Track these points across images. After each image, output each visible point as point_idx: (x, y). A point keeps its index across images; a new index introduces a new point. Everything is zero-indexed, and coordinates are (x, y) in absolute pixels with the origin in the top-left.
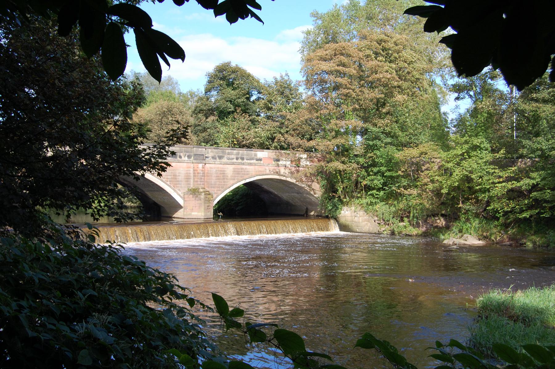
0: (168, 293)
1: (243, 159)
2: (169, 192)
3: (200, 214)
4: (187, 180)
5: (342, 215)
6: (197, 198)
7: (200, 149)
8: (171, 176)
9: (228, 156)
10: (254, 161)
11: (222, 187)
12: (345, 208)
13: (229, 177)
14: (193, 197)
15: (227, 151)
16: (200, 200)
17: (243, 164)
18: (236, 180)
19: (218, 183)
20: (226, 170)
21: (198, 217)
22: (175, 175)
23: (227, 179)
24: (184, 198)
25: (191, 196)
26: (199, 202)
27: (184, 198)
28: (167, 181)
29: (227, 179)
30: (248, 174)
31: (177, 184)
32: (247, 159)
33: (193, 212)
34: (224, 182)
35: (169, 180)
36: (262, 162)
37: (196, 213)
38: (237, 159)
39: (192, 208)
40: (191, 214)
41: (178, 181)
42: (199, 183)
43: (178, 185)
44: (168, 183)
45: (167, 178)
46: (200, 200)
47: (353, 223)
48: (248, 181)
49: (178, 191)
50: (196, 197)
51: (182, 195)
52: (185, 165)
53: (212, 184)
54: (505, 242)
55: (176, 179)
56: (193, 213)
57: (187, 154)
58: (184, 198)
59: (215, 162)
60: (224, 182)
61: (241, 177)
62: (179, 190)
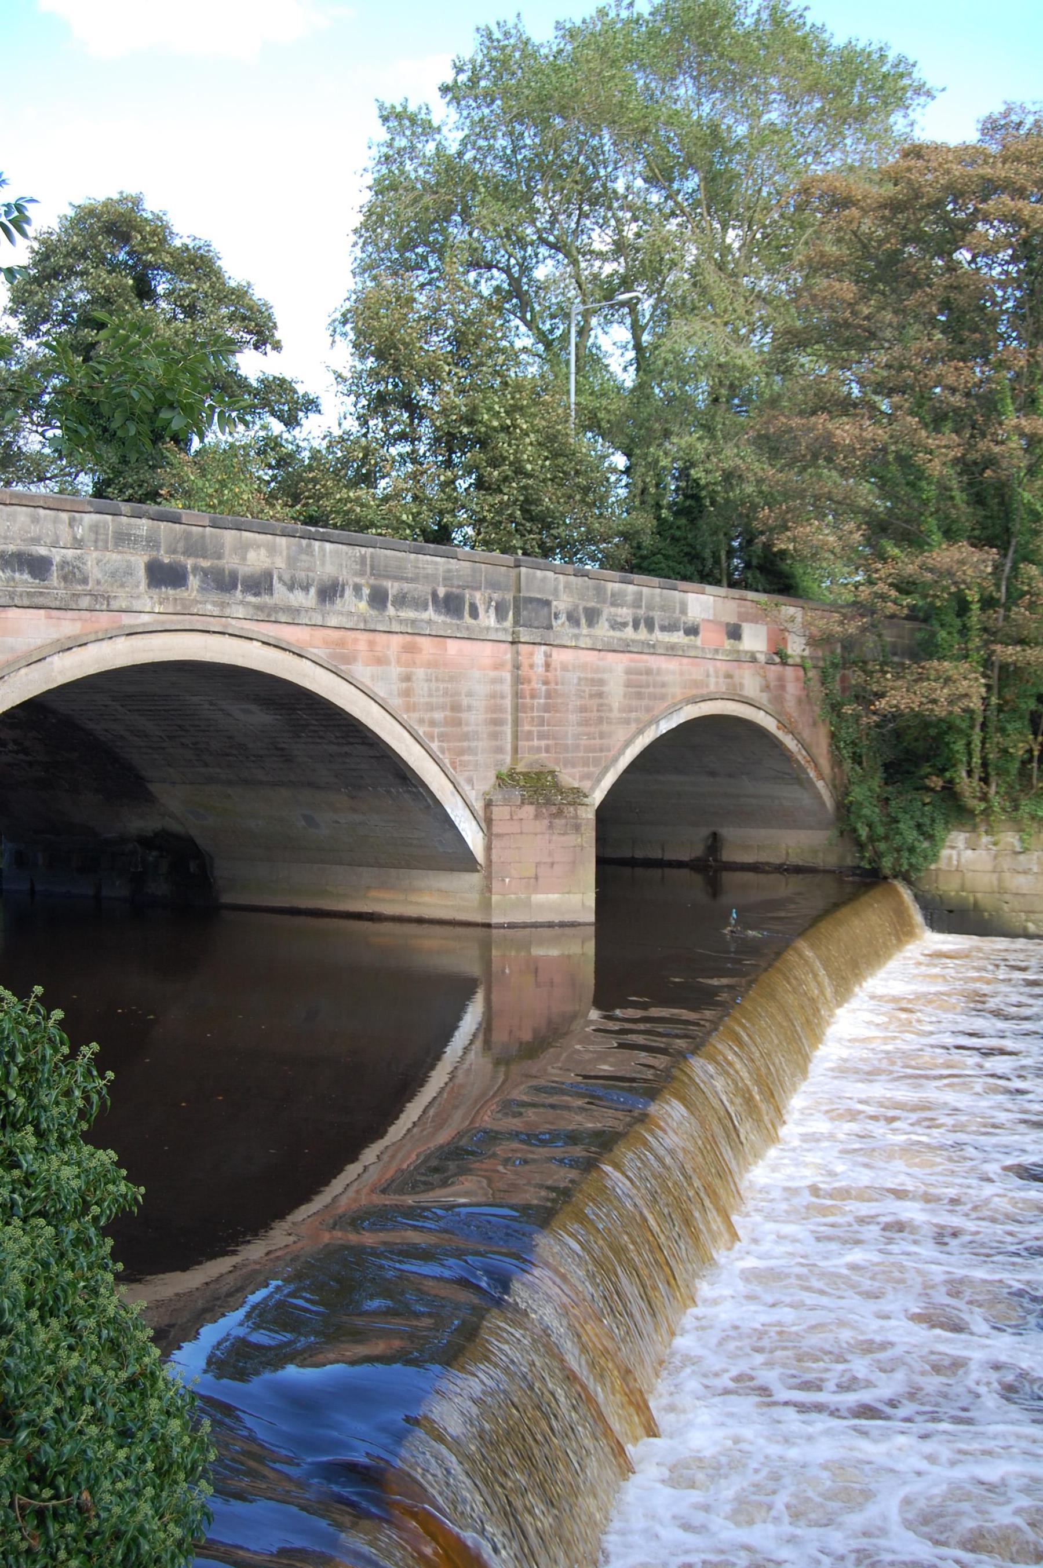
0: (142, 1190)
1: (650, 626)
2: (439, 795)
3: (575, 899)
4: (492, 728)
5: (942, 864)
6: (557, 822)
7: (539, 573)
8: (443, 708)
9: (613, 610)
10: (678, 638)
11: (596, 762)
12: (959, 838)
13: (615, 714)
14: (537, 817)
15: (610, 586)
16: (577, 828)
17: (651, 649)
18: (633, 727)
19: (584, 742)
20: (605, 676)
21: (568, 918)
22: (456, 708)
23: (609, 723)
24: (489, 821)
25: (529, 810)
26: (572, 839)
27: (489, 821)
28: (432, 738)
29: (609, 722)
30: (663, 697)
31: (461, 752)
32: (663, 629)
33: (536, 891)
34: (602, 736)
35: (436, 730)
36: (698, 641)
37: (554, 897)
38: (636, 626)
39: (531, 872)
40: (527, 904)
41: (466, 737)
42: (536, 743)
43: (466, 758)
44: (435, 746)
45: (432, 723)
46: (577, 828)
47: (1007, 897)
48: (665, 726)
49: (466, 788)
50: (554, 816)
51: (479, 806)
52: (484, 652)
53: (566, 749)
54: (853, 883)
55: (459, 723)
56: (538, 898)
57: (495, 596)
58: (487, 823)
59: (576, 637)
60: (602, 736)
61: (648, 710)
62: (470, 781)
